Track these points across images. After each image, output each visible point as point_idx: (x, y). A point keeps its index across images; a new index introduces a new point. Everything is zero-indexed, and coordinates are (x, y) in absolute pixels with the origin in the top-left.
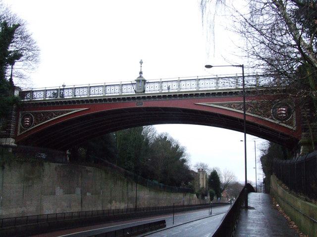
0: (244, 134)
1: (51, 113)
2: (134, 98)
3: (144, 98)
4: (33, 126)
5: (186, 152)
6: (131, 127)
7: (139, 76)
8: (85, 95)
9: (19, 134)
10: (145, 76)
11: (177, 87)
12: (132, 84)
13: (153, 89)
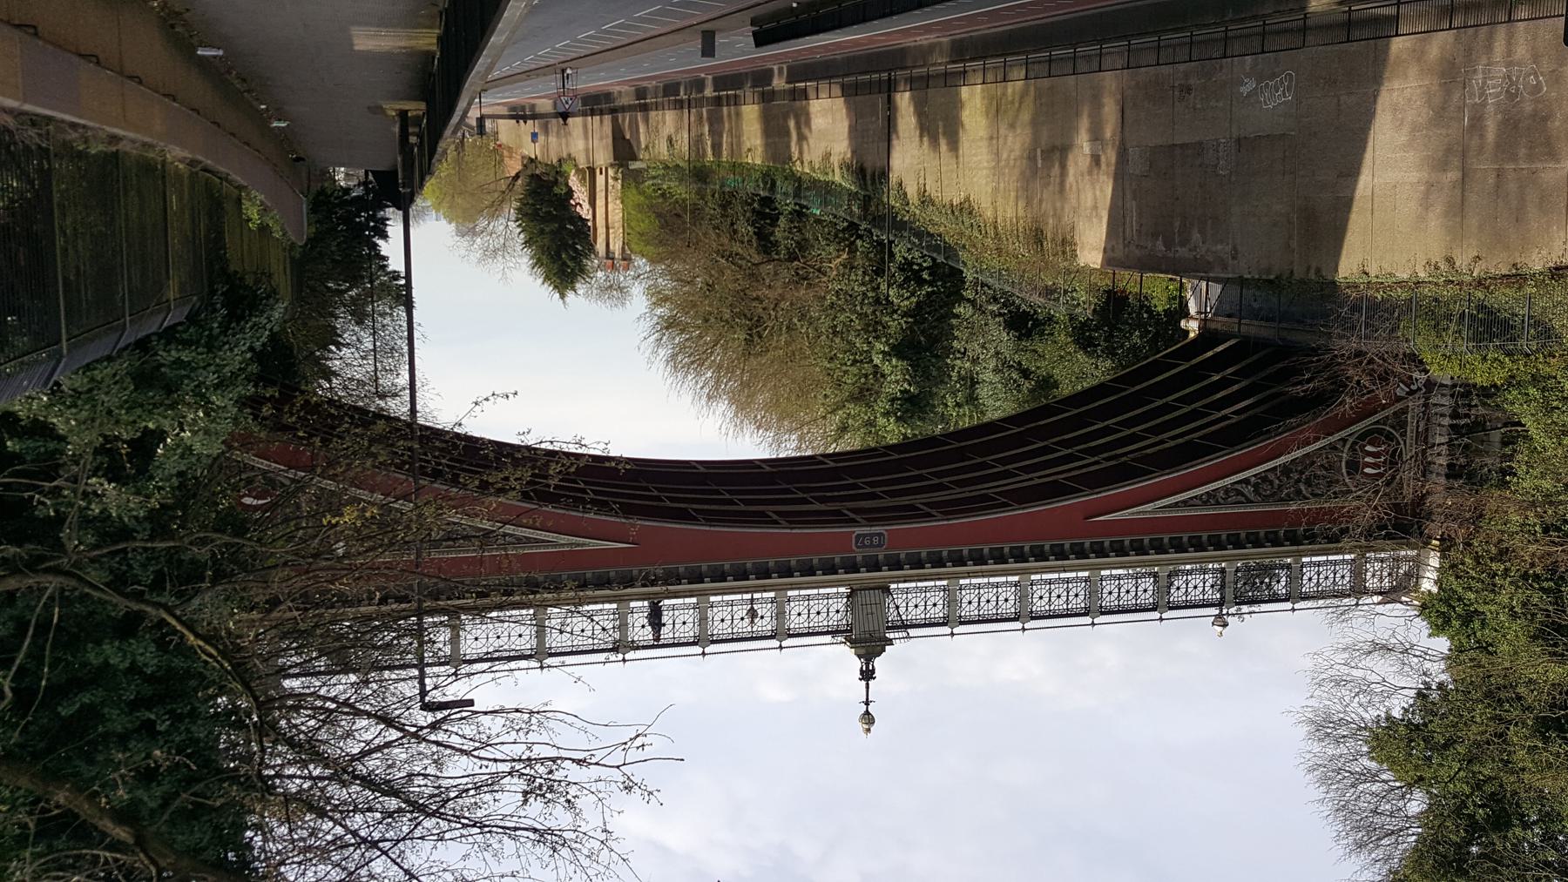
0: (421, 421)
1: (1266, 499)
2: (896, 565)
3: (853, 568)
7: (878, 663)
8: (1311, 564)
10: (846, 659)
11: (630, 620)
12: (904, 626)
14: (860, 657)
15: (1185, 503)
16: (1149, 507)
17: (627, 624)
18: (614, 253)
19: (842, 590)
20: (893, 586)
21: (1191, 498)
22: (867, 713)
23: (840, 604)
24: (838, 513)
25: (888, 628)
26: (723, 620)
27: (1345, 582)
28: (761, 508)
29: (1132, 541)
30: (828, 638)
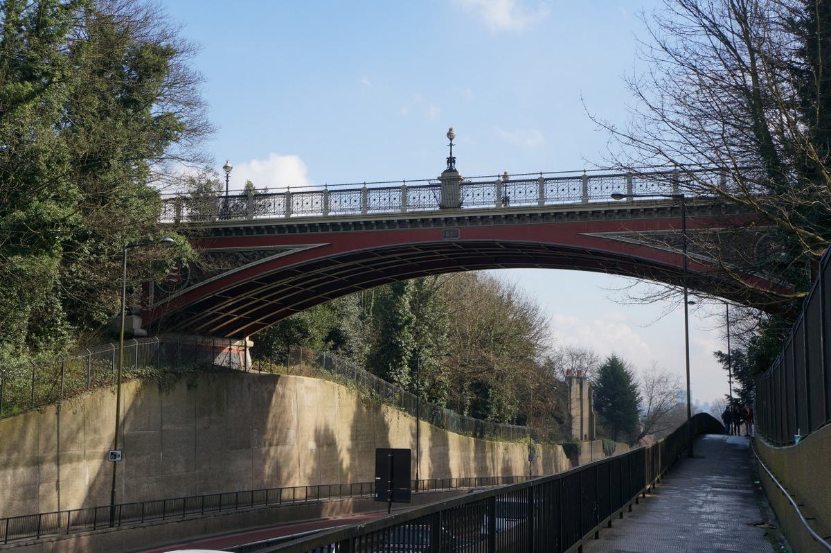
1: (232, 254)
4: (189, 285)
5: (542, 308)
6: (476, 269)
7: (445, 167)
9: (151, 305)
11: (538, 195)
12: (431, 186)
13: (308, 207)
14: (455, 170)
15: (277, 252)
16: (297, 250)
17: (583, 190)
18: (577, 382)
19: (465, 207)
20: (438, 209)
21: (273, 254)
22: (451, 139)
23: (467, 200)
24: (383, 254)
25: (440, 186)
26: (375, 200)
27: (296, 199)
28: (383, 257)
29: (395, 228)
30: (473, 181)
